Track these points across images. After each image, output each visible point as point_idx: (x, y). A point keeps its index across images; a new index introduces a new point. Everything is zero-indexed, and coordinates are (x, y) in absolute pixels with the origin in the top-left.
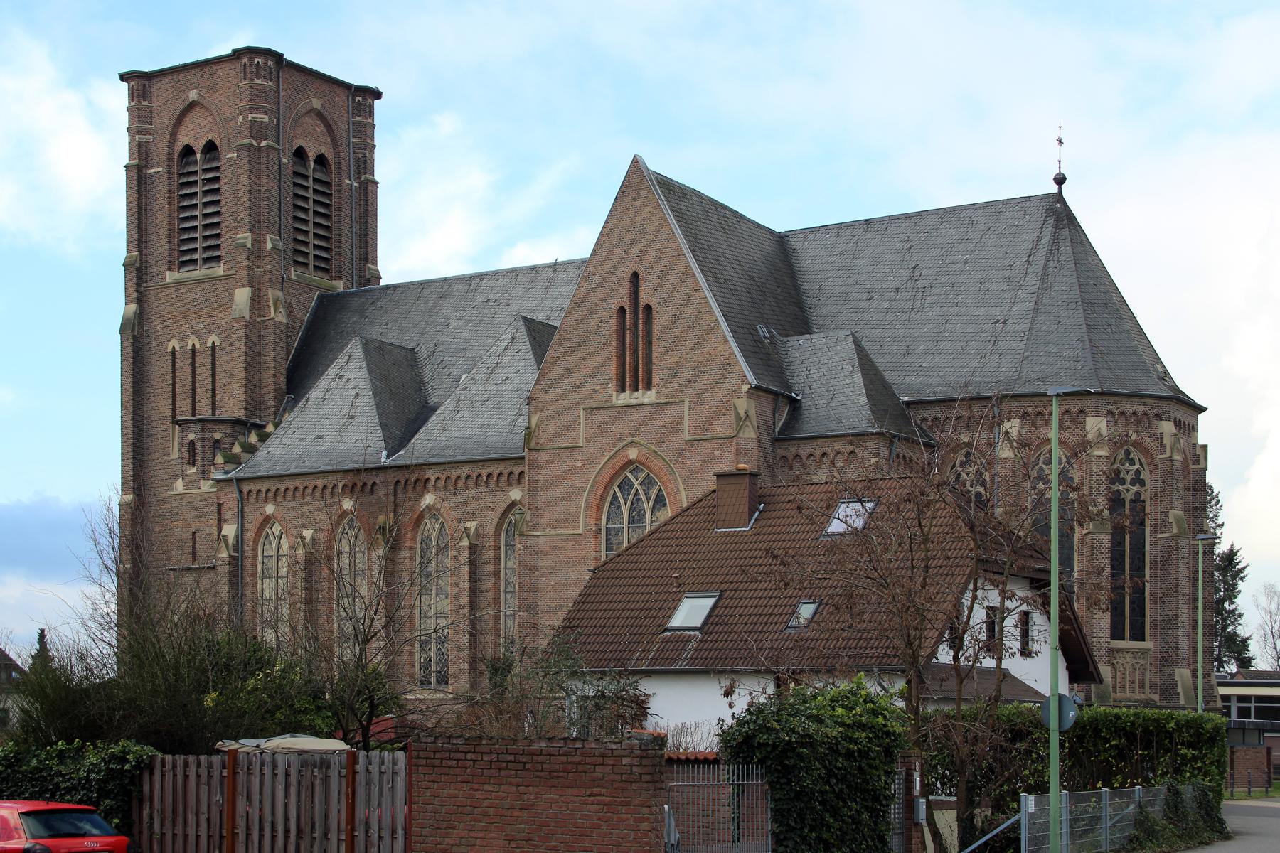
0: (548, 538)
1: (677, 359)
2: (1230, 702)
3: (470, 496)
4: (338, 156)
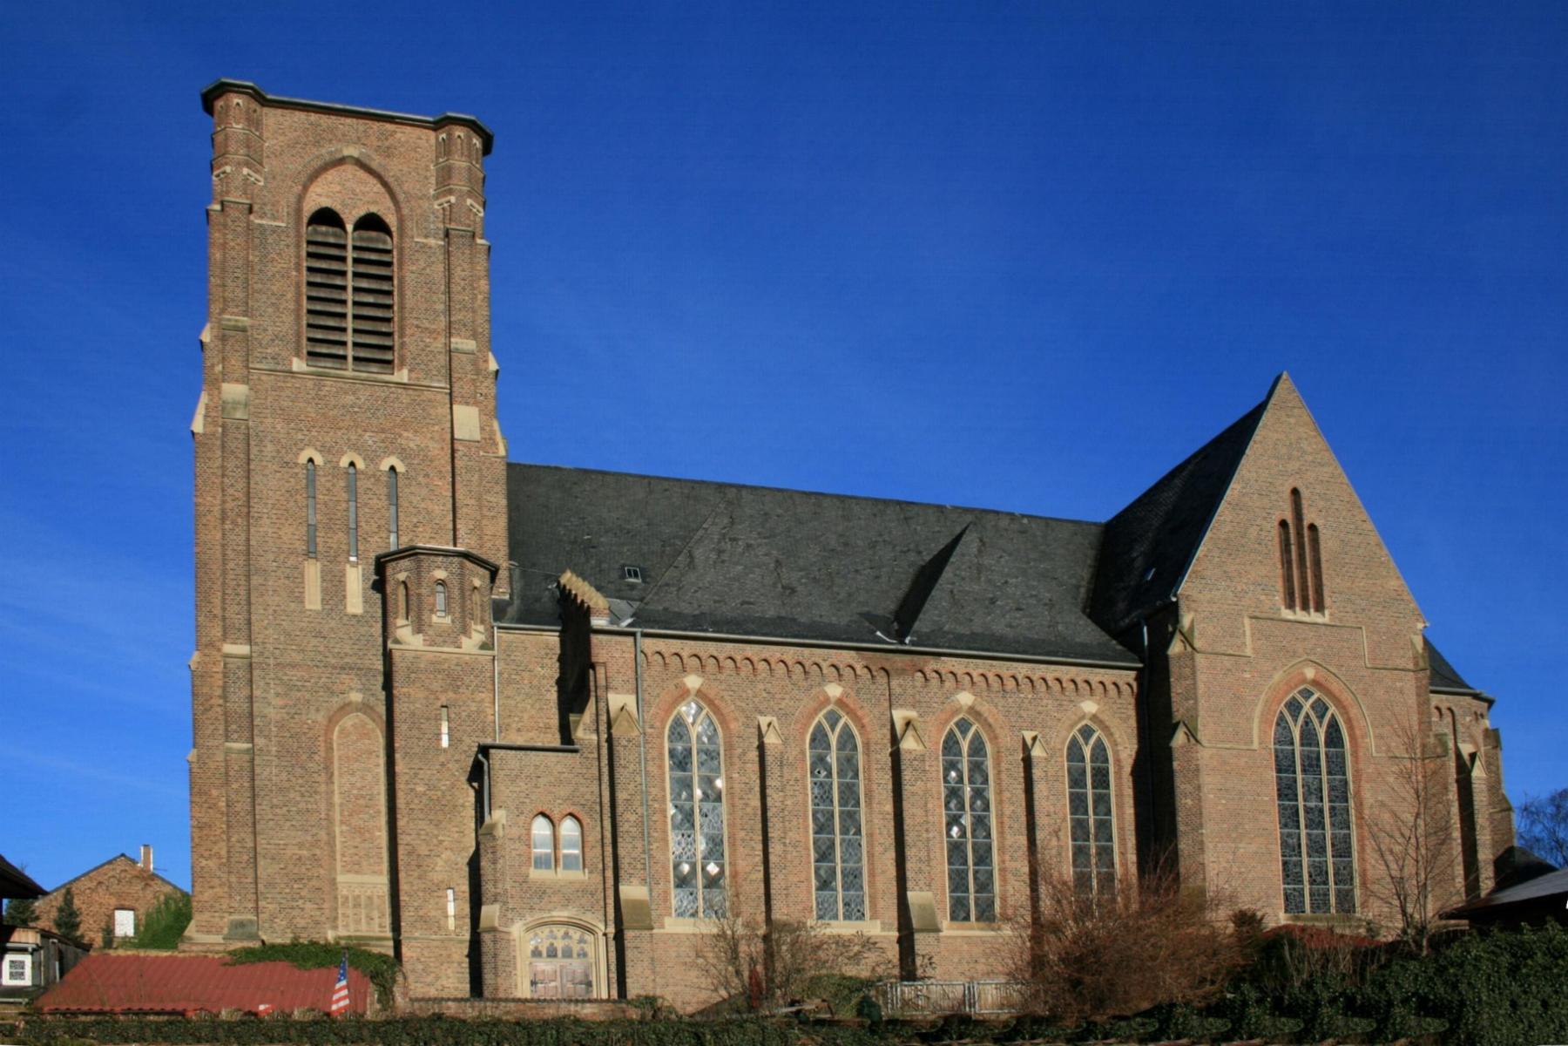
0: (1214, 751)
1: (1349, 584)
2: (978, 919)
3: (1026, 701)
4: (401, 221)
